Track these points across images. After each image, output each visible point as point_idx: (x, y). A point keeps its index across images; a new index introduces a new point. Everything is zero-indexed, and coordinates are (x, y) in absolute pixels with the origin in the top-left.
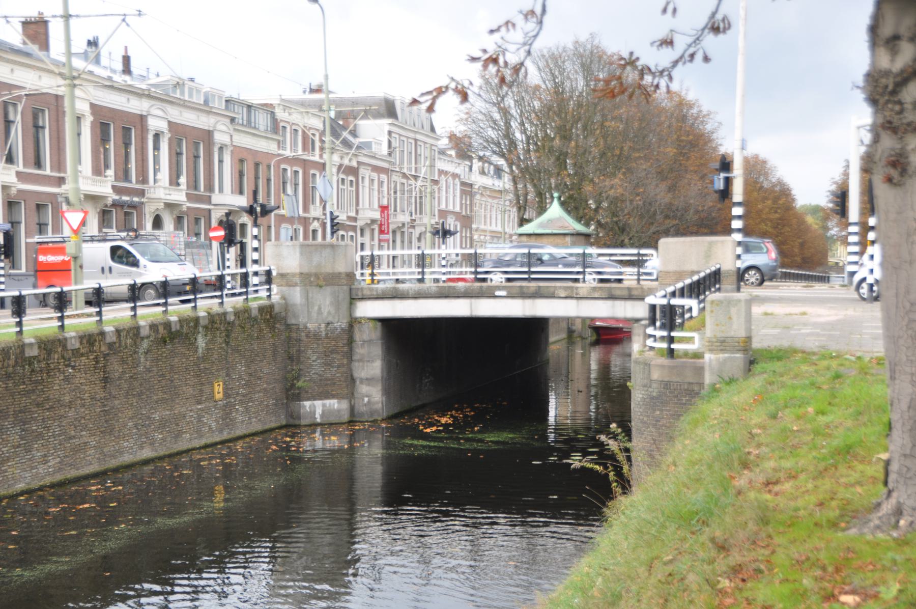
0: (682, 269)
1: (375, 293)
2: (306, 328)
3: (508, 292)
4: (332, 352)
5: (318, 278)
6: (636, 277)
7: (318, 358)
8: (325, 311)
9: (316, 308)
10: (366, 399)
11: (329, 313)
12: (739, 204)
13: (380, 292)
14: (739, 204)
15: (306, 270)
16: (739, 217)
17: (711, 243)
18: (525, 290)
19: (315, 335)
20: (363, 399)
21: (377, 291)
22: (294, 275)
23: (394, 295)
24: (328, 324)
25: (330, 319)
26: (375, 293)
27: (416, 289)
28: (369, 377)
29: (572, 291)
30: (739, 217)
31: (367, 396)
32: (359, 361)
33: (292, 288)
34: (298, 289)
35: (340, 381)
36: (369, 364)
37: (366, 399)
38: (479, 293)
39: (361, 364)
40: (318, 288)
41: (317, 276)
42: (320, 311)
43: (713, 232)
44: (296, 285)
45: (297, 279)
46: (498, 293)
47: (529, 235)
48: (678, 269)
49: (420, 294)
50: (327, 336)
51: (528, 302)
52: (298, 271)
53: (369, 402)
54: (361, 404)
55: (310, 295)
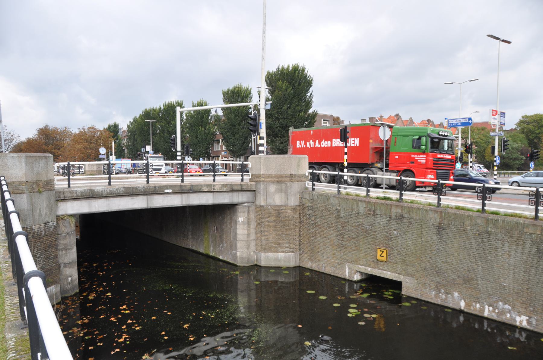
0: (283, 173)
1: (75, 195)
2: (32, 229)
3: (173, 190)
4: (49, 247)
5: (38, 185)
6: (108, 181)
7: (41, 254)
8: (43, 213)
9: (38, 211)
10: (70, 279)
11: (46, 214)
12: (179, 152)
13: (79, 194)
14: (179, 152)
15: (30, 179)
16: (178, 156)
17: (300, 158)
18: (184, 188)
19: (38, 235)
20: (67, 279)
21: (76, 193)
22: (20, 183)
23: (91, 195)
24: (46, 223)
25: (47, 219)
26: (75, 195)
27: (108, 190)
28: (70, 261)
29: (211, 187)
30: (178, 156)
31: (70, 277)
32: (62, 250)
33: (18, 195)
34: (24, 196)
35: (55, 269)
36: (70, 251)
37: (70, 279)
38: (153, 191)
39: (64, 252)
40: (39, 193)
41: (38, 183)
42: (40, 215)
43: (283, 154)
44: (22, 192)
45: (24, 187)
46: (166, 191)
47: (407, 136)
48: (279, 173)
49: (111, 194)
50: (46, 235)
51: (185, 196)
52: (24, 180)
53: (71, 280)
54: (66, 284)
55: (34, 201)
